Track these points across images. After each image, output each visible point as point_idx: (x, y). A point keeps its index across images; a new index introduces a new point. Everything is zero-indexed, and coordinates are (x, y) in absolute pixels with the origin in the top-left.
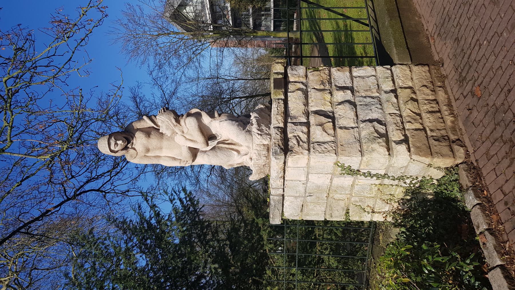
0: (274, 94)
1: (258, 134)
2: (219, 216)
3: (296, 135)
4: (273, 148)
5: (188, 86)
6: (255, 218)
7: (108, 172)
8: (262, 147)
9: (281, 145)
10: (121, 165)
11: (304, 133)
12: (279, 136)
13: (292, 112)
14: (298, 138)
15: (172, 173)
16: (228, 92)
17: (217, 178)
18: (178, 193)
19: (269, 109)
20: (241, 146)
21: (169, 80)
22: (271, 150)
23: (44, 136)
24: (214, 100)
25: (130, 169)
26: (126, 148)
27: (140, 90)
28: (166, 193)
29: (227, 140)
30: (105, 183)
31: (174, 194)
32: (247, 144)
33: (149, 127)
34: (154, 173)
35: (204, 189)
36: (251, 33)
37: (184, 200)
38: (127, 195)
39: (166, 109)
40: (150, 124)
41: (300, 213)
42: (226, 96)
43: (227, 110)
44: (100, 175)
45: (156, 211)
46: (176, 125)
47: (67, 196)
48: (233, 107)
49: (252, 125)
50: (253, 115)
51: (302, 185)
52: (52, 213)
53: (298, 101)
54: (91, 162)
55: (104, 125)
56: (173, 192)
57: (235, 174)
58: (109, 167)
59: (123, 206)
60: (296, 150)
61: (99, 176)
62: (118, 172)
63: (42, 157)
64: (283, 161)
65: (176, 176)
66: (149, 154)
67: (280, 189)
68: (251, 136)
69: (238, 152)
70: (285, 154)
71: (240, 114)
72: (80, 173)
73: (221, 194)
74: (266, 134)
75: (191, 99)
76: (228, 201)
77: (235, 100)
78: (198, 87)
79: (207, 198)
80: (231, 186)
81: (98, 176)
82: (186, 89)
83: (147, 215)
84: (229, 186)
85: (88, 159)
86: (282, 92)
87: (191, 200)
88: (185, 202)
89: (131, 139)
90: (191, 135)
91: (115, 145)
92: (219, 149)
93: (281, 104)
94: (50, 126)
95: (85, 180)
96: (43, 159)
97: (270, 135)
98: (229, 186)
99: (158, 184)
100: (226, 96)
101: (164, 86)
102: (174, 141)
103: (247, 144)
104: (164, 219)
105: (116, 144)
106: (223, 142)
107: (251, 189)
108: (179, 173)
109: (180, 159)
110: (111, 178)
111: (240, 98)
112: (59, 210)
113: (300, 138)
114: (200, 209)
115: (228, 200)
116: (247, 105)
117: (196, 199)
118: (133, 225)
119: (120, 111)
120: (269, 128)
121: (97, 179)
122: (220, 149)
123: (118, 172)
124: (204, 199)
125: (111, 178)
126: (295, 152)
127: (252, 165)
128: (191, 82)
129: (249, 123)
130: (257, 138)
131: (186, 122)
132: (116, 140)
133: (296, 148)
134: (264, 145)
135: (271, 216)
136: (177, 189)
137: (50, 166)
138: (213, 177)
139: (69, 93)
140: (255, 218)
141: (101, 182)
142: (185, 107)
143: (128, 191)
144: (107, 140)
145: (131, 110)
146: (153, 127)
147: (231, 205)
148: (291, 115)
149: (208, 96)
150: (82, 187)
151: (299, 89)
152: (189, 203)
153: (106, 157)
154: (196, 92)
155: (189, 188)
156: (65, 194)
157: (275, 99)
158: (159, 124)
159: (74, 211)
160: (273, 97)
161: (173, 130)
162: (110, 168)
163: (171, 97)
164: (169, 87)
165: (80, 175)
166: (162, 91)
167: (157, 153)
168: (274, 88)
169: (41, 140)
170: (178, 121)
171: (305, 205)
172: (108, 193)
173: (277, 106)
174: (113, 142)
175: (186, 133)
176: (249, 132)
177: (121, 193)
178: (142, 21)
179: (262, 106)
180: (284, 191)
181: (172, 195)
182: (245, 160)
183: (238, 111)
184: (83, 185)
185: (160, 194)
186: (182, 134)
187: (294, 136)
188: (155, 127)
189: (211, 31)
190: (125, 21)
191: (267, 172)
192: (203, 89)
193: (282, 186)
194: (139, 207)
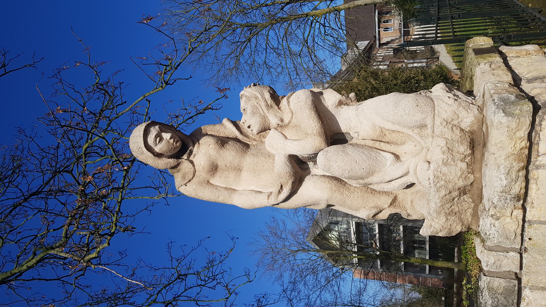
36: (402, 258)
66: (216, 181)
67: (512, 254)
89: (191, 144)
105: (159, 136)
132: (161, 131)
174: (154, 131)
178: (283, 236)
188: (240, 137)
189: (355, 252)
190: (268, 233)
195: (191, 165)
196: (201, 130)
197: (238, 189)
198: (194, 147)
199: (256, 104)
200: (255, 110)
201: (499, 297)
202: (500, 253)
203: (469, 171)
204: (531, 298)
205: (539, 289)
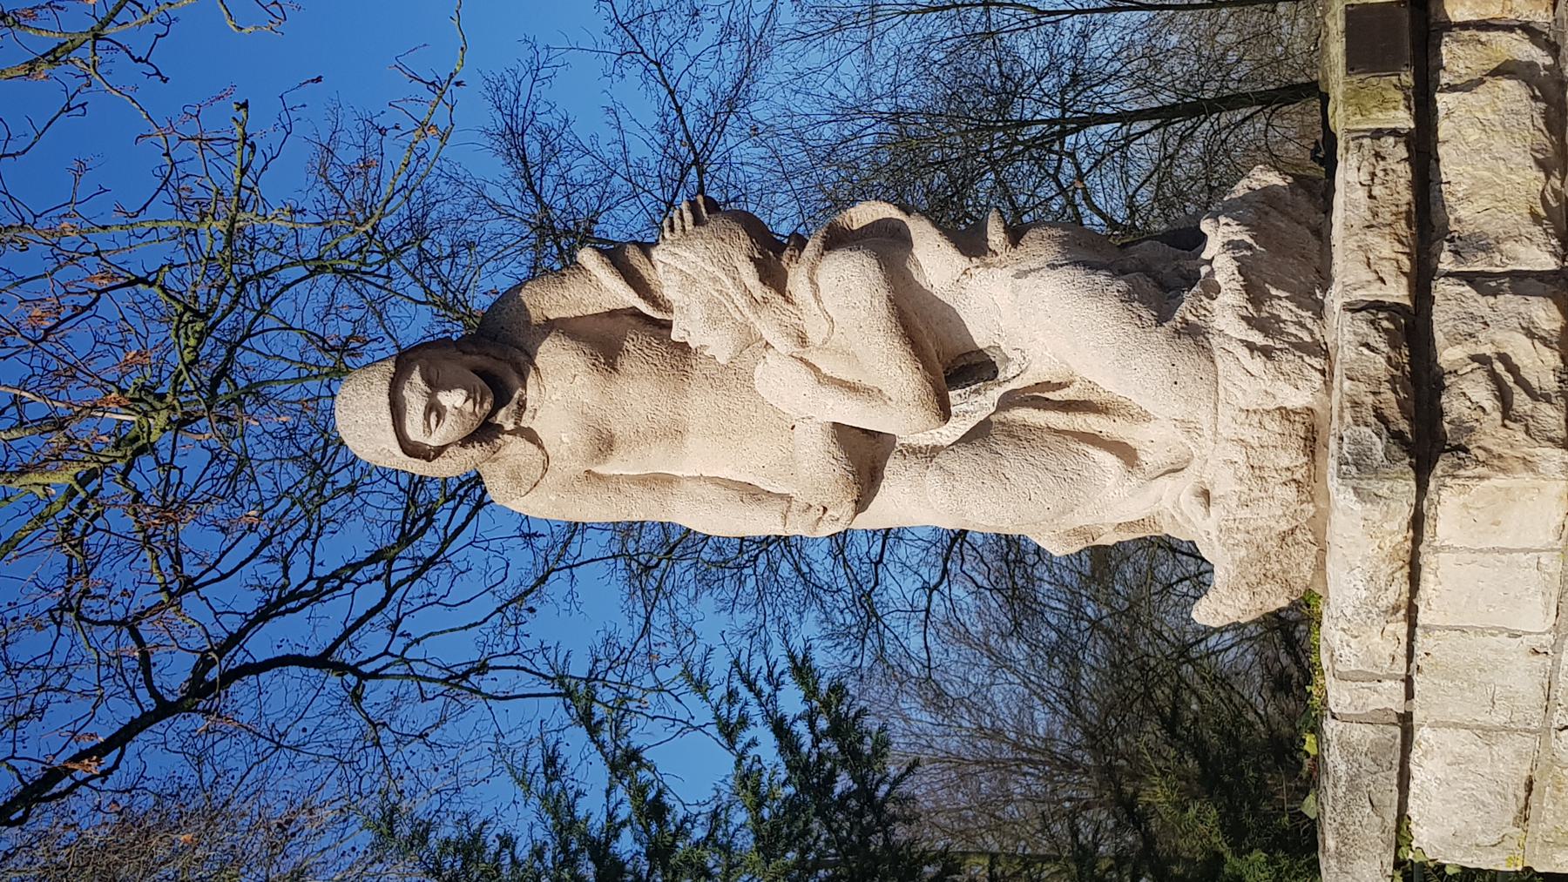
0: (1346, 102)
1: (1251, 347)
2: (998, 826)
3: (1488, 350)
4: (1342, 433)
5: (815, 57)
6: (1224, 848)
7: (374, 559)
8: (1274, 426)
9: (1392, 411)
10: (442, 517)
11: (1545, 342)
12: (1381, 360)
13: (1462, 213)
14: (1499, 367)
15: (722, 565)
16: (1048, 84)
17: (984, 599)
18: (767, 689)
19: (1320, 192)
20: (1146, 417)
21: (707, 25)
22: (1333, 444)
23: (37, 361)
24: (963, 134)
25: (494, 545)
26: (485, 432)
27: (544, 92)
28: (700, 687)
29: (1060, 386)
30: (360, 622)
31: (744, 693)
32: (1179, 410)
33: (612, 314)
34: (621, 563)
35: (905, 662)
37: (801, 727)
38: (478, 692)
39: (707, 210)
40: (615, 292)
41: (1513, 830)
42: (1035, 110)
43: (1043, 192)
44: (335, 575)
45: (642, 791)
46: (766, 301)
47: (154, 693)
48: (1081, 176)
49: (1213, 290)
50: (1218, 235)
51: (1525, 661)
52: (77, 784)
53: (1500, 144)
54: (286, 503)
55: (346, 296)
56: (737, 683)
57: (1092, 578)
58: (377, 531)
59: (451, 753)
60: (1488, 442)
61: (327, 579)
62: (431, 562)
63: (34, 477)
64: (1406, 513)
65: (742, 583)
67: (1387, 684)
68: (1205, 361)
69: (1126, 453)
70: (1422, 472)
71: (1120, 215)
72: (225, 567)
73: (1004, 694)
74: (1301, 347)
75: (828, 132)
76: (1050, 738)
77: (1091, 130)
78: (869, 60)
79: (926, 717)
80: (1064, 652)
81: (322, 581)
82: (800, 75)
83: (592, 809)
84: (1053, 651)
85: (265, 483)
86: (1400, 87)
87: (841, 728)
88: (807, 740)
89: (515, 380)
90: (849, 356)
91: (427, 417)
92: (1011, 435)
93: (1391, 163)
94: (84, 309)
95: (251, 602)
96: (39, 491)
97: (1326, 354)
98: (1053, 651)
99: (646, 631)
100: (1035, 110)
101: (679, 62)
102: (752, 389)
103: (1179, 410)
104: (687, 835)
106: (1034, 397)
107: (1187, 669)
108: (761, 568)
109: (782, 496)
110: (390, 591)
111: (1125, 118)
112: (116, 766)
113: (1513, 369)
114: (897, 782)
115: (1050, 732)
116: (1163, 170)
117: (871, 723)
118: (514, 861)
119: (434, 215)
120: (1319, 311)
121: (316, 596)
122: (1012, 433)
123: (431, 562)
124: (906, 719)
125: (390, 591)
126: (1482, 455)
127: (1214, 534)
128: (832, 31)
129: (1191, 279)
130: (1240, 374)
131: (821, 282)
132: (434, 385)
133: (1492, 434)
134: (1285, 413)
135: (1331, 842)
136: (758, 662)
137: (78, 528)
138: (958, 591)
139: (178, 124)
140: (1224, 848)
141: (331, 615)
142: (797, 183)
143: (482, 668)
144: (385, 387)
145: (494, 205)
146: (635, 313)
147: (1070, 765)
148: (1453, 227)
149: (931, 116)
150: (235, 639)
151: (1506, 70)
152: (830, 746)
153: (363, 477)
154: (861, 93)
155: (827, 661)
156: (149, 684)
157: (1357, 136)
158: (670, 292)
159: (188, 773)
160: (1340, 120)
161: (747, 328)
162: (384, 536)
163: (717, 126)
164: (707, 61)
165: (224, 577)
166: (664, 92)
167: (656, 460)
168: (1351, 67)
169: (23, 385)
170: (772, 276)
171: (1544, 785)
172: (375, 675)
173: (1365, 177)
174: (415, 397)
175: (819, 343)
176: (1195, 334)
177: (445, 681)
179: (1274, 179)
180: (1410, 695)
181: (732, 696)
182: (1167, 504)
183: (1108, 194)
184: (242, 633)
185: (659, 689)
186: (797, 351)
187: (1474, 358)
191: (1303, 575)
192: (902, 77)
193: (1402, 662)
194: (550, 760)
195: (532, 448)
196: (526, 310)
197: (679, 474)
198: (525, 388)
199: (716, 294)
200: (716, 313)
201: (1362, 759)
202: (1364, 685)
203: (1304, 498)
204: (1431, 741)
205: (1449, 727)
